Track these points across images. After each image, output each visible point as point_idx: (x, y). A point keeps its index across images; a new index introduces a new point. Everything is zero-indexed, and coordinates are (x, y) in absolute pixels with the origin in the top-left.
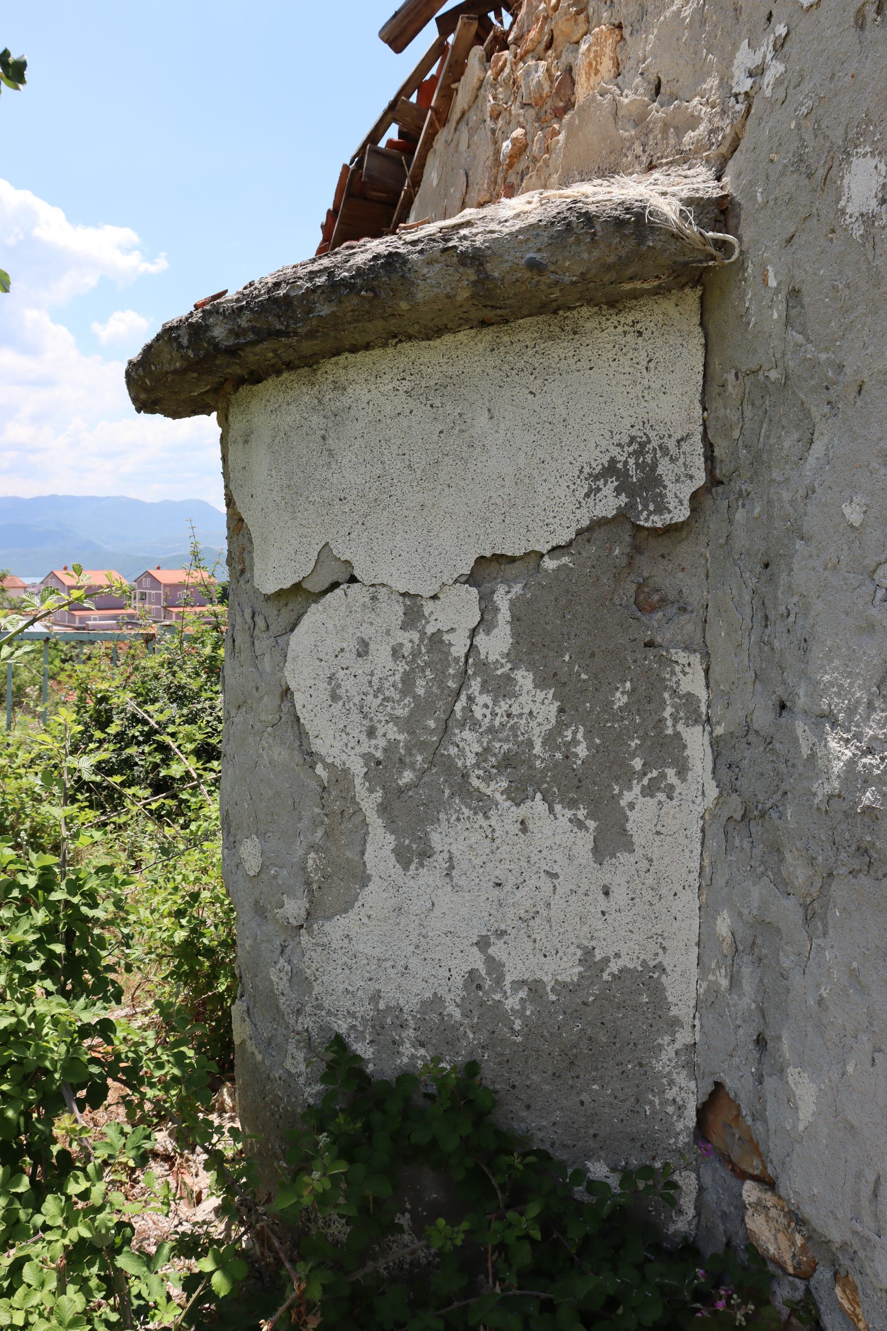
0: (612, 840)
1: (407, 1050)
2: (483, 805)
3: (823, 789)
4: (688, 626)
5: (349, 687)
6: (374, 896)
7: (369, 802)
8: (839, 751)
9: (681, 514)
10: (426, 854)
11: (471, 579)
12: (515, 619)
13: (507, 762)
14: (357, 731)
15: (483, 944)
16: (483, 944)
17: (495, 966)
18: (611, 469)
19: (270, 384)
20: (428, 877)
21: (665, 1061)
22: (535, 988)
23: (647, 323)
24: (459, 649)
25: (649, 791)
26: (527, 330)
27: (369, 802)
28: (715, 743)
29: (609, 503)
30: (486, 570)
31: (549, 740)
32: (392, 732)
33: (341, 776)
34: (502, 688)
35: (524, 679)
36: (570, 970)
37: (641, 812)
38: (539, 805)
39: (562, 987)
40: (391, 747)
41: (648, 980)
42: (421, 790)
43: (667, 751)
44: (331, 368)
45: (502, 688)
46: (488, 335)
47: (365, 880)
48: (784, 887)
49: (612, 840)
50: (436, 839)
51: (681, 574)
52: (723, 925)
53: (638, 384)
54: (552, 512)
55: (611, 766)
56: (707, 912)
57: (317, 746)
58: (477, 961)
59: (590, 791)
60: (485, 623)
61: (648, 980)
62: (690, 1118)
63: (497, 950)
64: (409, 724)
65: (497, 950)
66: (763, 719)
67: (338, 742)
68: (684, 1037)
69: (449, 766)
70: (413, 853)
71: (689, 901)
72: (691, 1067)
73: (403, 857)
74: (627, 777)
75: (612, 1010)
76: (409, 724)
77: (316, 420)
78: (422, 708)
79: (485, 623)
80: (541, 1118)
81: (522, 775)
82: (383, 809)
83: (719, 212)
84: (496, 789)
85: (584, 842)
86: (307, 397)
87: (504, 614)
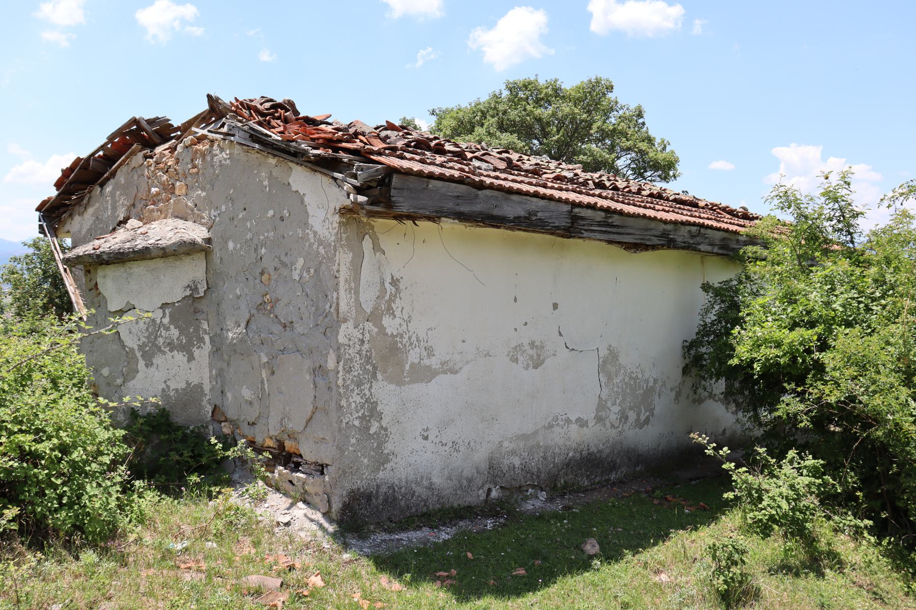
0: (191, 358)
1: (149, 408)
2: (164, 353)
3: (228, 341)
4: (204, 316)
5: (134, 330)
6: (140, 375)
7: (139, 354)
8: (230, 335)
9: (202, 294)
10: (152, 364)
11: (161, 308)
12: (170, 315)
13: (169, 344)
14: (136, 339)
15: (165, 382)
16: (165, 382)
17: (168, 387)
18: (188, 286)
19: (112, 266)
20: (153, 369)
21: (204, 403)
22: (177, 390)
23: (195, 258)
24: (158, 322)
25: (198, 348)
26: (171, 259)
27: (139, 354)
28: (210, 338)
29: (188, 293)
30: (164, 306)
31: (177, 339)
32: (144, 339)
33: (132, 350)
34: (168, 329)
35: (172, 327)
36: (183, 385)
37: (196, 352)
38: (176, 352)
39: (182, 389)
40: (144, 343)
41: (200, 386)
42: (150, 351)
43: (201, 340)
44: (128, 264)
45: (168, 329)
46: (163, 259)
47: (138, 372)
48: (224, 361)
49: (191, 358)
50: (154, 361)
51: (202, 305)
52: (214, 372)
53: (195, 270)
54: (177, 294)
55: (190, 344)
56: (211, 371)
57: (126, 344)
58: (164, 386)
59: (186, 348)
60: (164, 316)
61: (200, 386)
62: (210, 414)
63: (168, 383)
64: (147, 338)
65: (168, 383)
66: (219, 332)
67: (131, 342)
68: (208, 397)
69: (157, 346)
70: (149, 364)
71: (207, 369)
72: (210, 403)
73: (147, 366)
74: (193, 346)
75: (193, 392)
76: (147, 338)
77: (125, 275)
78: (151, 334)
79: (164, 316)
80: (178, 419)
81: (172, 346)
82: (142, 356)
83: (208, 241)
84: (167, 350)
85: (185, 359)
86: (122, 269)
87: (168, 314)
